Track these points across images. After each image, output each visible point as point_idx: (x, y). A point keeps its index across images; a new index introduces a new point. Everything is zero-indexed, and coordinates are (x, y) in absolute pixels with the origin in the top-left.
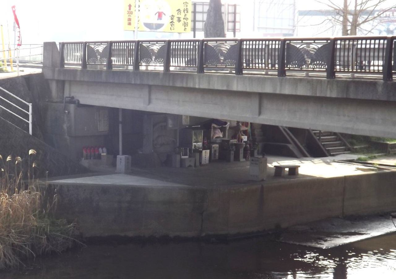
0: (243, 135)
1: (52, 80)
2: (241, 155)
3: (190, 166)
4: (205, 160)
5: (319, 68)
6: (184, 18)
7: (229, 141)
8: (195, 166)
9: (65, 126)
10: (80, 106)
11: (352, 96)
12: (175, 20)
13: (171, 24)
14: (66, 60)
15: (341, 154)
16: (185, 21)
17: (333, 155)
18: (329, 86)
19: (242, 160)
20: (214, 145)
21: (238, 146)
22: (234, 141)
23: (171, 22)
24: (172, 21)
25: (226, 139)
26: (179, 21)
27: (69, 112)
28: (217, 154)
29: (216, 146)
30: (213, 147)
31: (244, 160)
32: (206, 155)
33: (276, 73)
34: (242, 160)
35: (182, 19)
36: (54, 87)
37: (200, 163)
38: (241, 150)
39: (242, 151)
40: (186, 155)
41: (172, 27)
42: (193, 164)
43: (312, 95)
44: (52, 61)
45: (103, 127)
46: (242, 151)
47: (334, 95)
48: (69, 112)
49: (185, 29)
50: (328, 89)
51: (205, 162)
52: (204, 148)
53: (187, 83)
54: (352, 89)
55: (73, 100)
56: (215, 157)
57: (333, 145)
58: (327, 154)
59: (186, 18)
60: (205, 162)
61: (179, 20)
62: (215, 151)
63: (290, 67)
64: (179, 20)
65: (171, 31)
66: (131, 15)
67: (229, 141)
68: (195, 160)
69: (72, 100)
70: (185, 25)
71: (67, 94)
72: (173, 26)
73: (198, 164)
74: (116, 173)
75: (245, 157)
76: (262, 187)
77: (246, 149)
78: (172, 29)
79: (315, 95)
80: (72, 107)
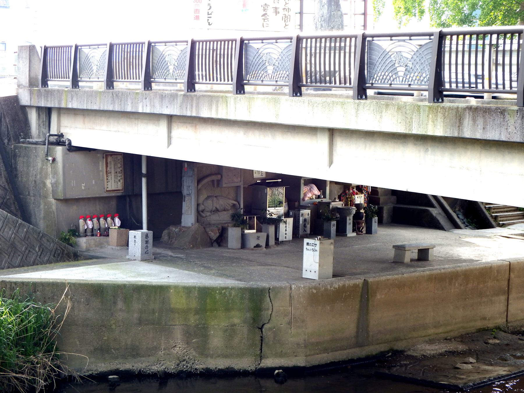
0: (357, 194)
1: (31, 107)
2: (349, 227)
3: (258, 246)
4: (286, 234)
5: (419, 85)
6: (284, 9)
7: (329, 204)
8: (267, 245)
9: (49, 183)
10: (73, 149)
11: (467, 134)
12: (270, 12)
13: (263, 17)
14: (199, 78)
15: (514, 224)
16: (286, 13)
17: (503, 226)
18: (431, 116)
19: (351, 234)
20: (303, 211)
21: (342, 213)
22: (339, 204)
23: (263, 16)
24: (265, 12)
25: (326, 200)
26: (276, 13)
27: (54, 160)
28: (308, 226)
29: (306, 213)
30: (302, 215)
31: (355, 234)
32: (286, 230)
33: (351, 93)
34: (351, 234)
35: (280, 10)
36: (33, 117)
37: (277, 239)
38: (348, 218)
39: (350, 220)
40: (251, 228)
41: (265, 23)
42: (263, 243)
43: (405, 132)
44: (29, 75)
45: (114, 184)
46: (350, 220)
47: (439, 132)
48: (54, 160)
49: (286, 25)
50: (430, 122)
51: (286, 238)
52: (287, 215)
53: (217, 110)
54: (467, 122)
55: (62, 139)
56: (305, 231)
57: (505, 209)
58: (494, 223)
59: (287, 8)
60: (286, 238)
61: (277, 12)
62: (305, 220)
63: (374, 82)
64: (277, 12)
65: (263, 29)
66: (199, 3)
67: (329, 204)
68: (268, 237)
69: (60, 140)
70: (286, 18)
71: (54, 130)
72: (266, 20)
73: (272, 241)
74: (129, 260)
75: (356, 229)
76: (366, 282)
77: (357, 217)
78: (265, 25)
79: (410, 132)
80: (59, 151)
